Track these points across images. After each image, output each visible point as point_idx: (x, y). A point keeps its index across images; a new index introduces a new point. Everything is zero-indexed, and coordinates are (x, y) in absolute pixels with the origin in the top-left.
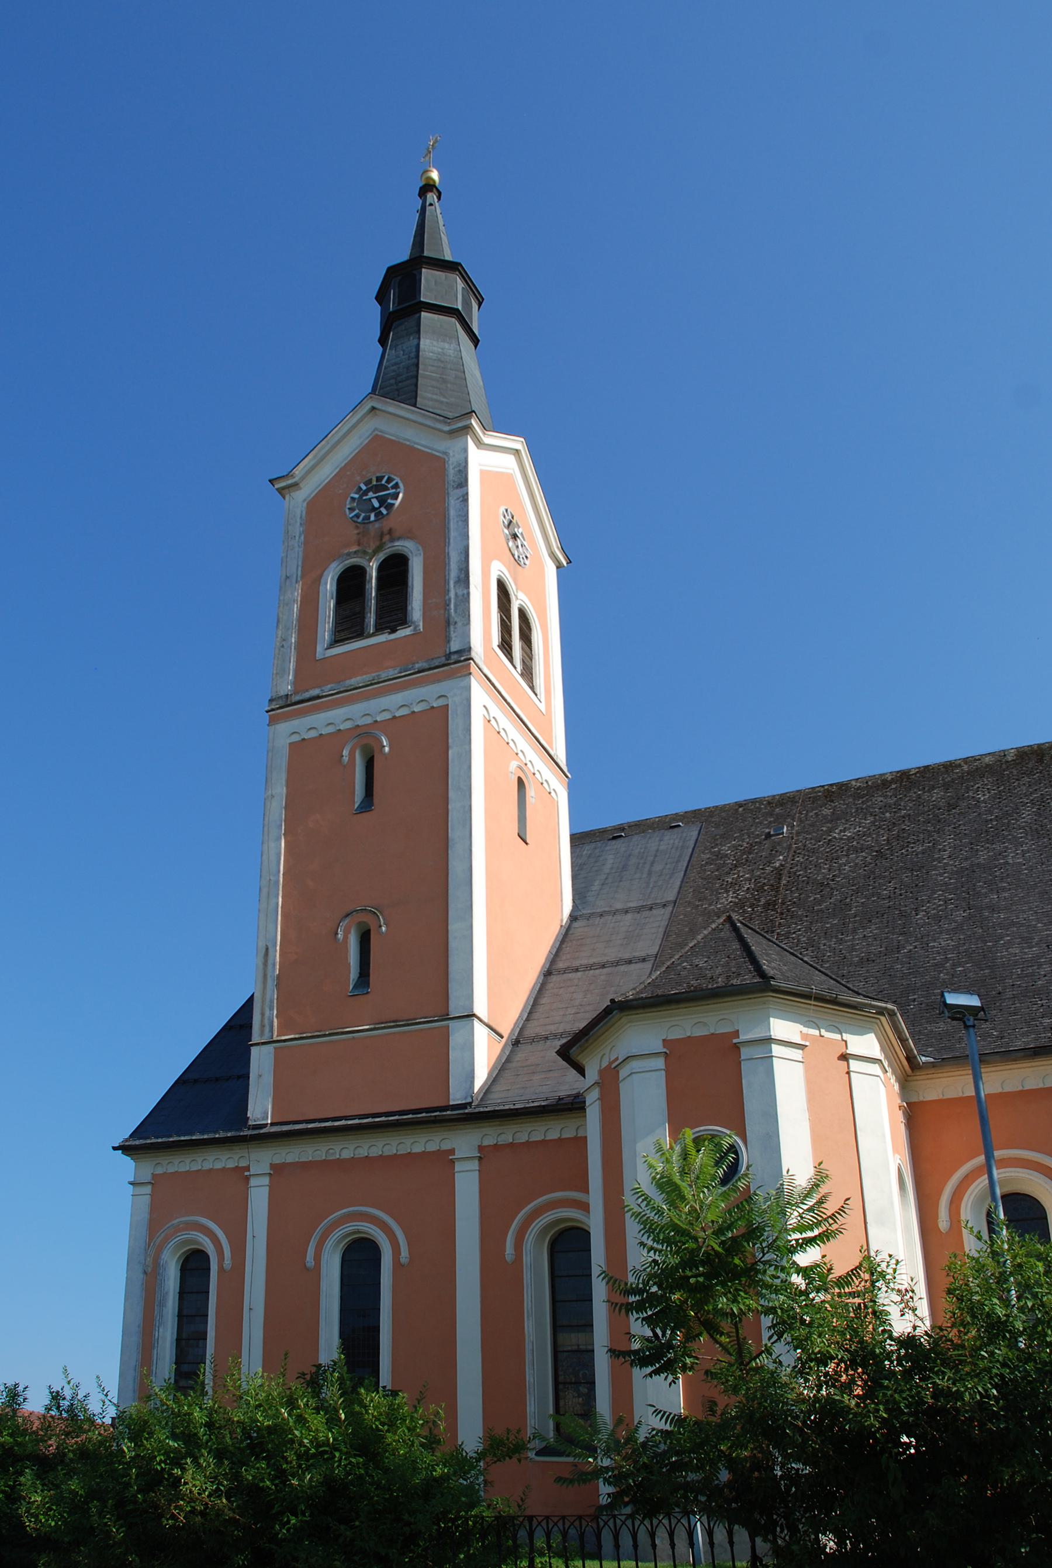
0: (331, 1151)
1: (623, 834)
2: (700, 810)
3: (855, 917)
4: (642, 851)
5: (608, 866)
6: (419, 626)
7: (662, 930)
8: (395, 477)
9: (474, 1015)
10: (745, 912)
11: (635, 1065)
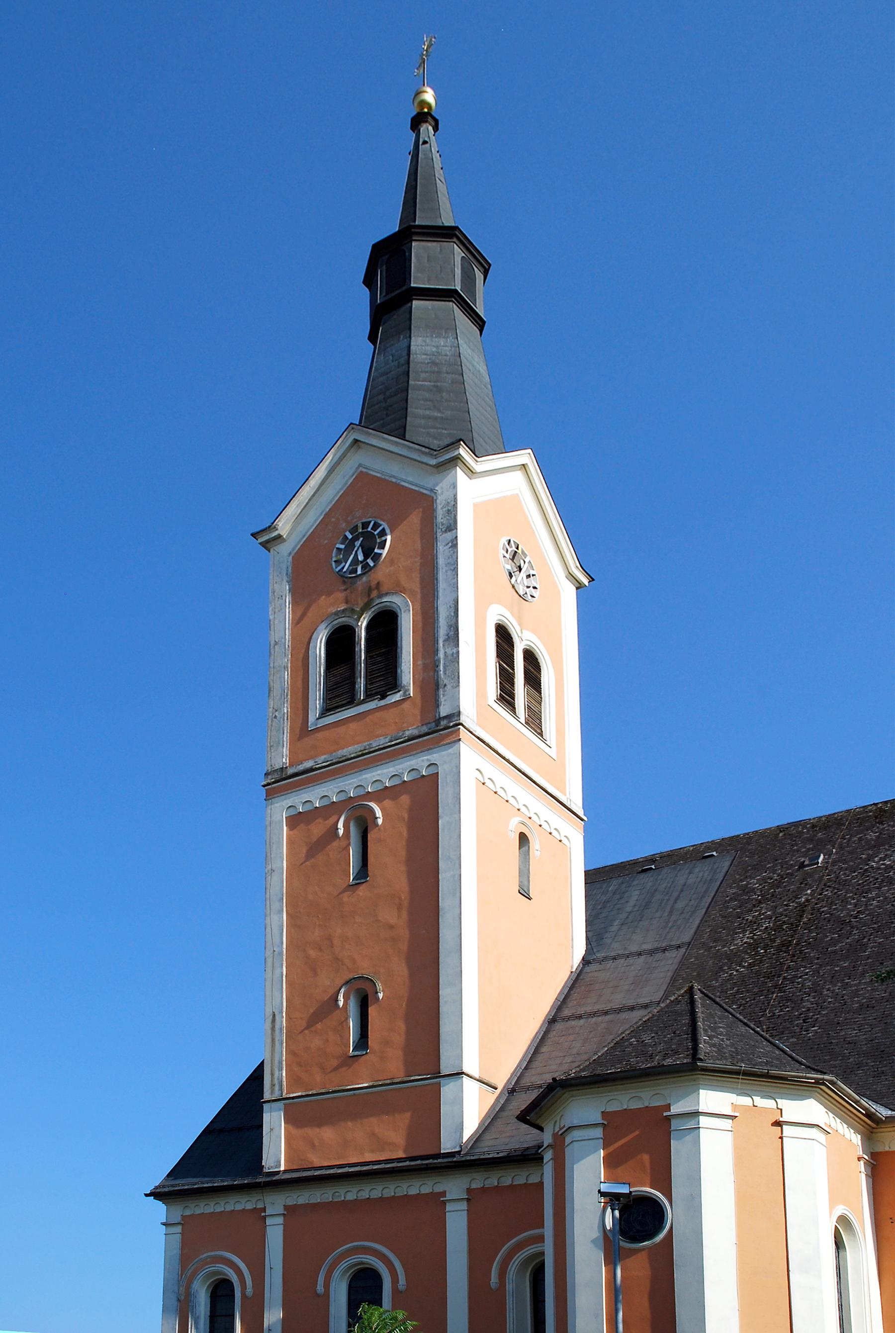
0: (337, 1194)
1: (653, 867)
2: (738, 836)
3: (868, 958)
4: (669, 885)
5: (632, 903)
6: (409, 690)
7: (670, 974)
8: (382, 523)
9: (463, 1073)
10: (757, 953)
11: (576, 1134)
